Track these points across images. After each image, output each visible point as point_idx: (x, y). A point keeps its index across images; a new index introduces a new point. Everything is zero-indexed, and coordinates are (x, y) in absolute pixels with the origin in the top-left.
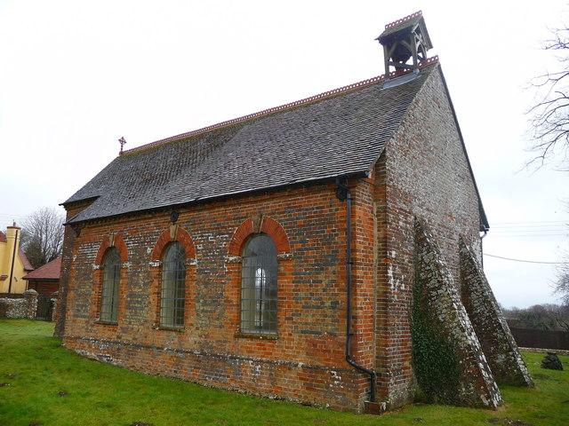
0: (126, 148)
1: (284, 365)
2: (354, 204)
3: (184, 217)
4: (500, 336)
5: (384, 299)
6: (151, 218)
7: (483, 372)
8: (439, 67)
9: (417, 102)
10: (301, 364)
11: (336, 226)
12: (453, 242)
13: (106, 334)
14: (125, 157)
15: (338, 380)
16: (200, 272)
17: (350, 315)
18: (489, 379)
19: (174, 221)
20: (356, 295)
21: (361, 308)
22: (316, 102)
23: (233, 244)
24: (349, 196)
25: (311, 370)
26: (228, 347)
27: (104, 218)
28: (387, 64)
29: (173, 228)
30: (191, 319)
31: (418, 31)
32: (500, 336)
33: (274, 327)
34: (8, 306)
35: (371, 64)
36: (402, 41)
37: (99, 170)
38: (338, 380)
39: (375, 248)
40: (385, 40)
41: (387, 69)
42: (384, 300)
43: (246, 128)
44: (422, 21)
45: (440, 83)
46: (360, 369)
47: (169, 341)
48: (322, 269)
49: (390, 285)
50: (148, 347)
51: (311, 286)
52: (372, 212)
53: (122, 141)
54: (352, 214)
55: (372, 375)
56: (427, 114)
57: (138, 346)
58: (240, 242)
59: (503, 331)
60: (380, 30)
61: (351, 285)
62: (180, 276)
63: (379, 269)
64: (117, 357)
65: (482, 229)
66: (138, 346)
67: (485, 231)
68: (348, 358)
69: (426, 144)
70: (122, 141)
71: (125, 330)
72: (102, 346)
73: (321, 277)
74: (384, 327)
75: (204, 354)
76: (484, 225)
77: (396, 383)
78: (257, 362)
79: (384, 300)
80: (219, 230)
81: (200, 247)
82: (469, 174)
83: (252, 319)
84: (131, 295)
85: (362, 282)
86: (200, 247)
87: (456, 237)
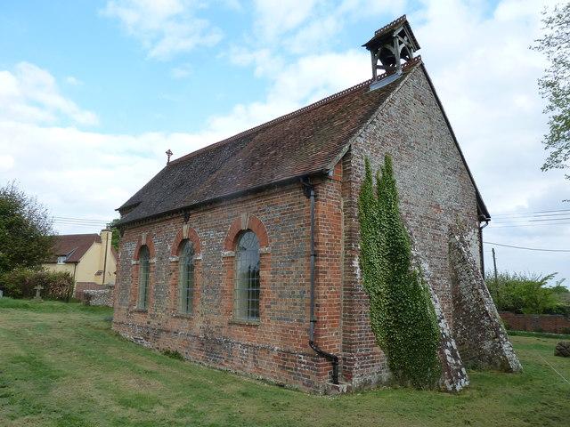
0: (173, 159)
1: (264, 348)
2: (317, 200)
3: (194, 217)
4: (487, 323)
5: (350, 289)
6: (170, 219)
7: (449, 359)
8: (422, 65)
9: (392, 101)
10: (276, 348)
11: (304, 222)
12: (439, 232)
13: (140, 319)
14: (172, 166)
15: (304, 363)
16: (204, 266)
17: (314, 306)
18: (457, 365)
19: (187, 220)
20: (319, 285)
21: (325, 297)
22: (343, 97)
23: (227, 240)
24: (312, 193)
25: (285, 355)
26: (224, 331)
27: (143, 219)
28: (375, 67)
29: (185, 227)
30: (199, 307)
31: (402, 34)
32: (487, 323)
33: (256, 314)
34: (91, 296)
35: (358, 69)
36: (391, 45)
37: (156, 174)
38: (304, 363)
39: (342, 241)
40: (371, 46)
41: (374, 72)
42: (349, 290)
43: (258, 137)
44: (406, 24)
45: (424, 81)
46: (322, 354)
47: (183, 327)
48: (293, 261)
49: (356, 275)
50: (168, 332)
51: (284, 277)
52: (339, 207)
53: (169, 153)
54: (315, 210)
55: (336, 359)
56: (406, 111)
57: (161, 331)
58: (232, 238)
59: (490, 319)
60: (370, 36)
61: (315, 274)
62: (190, 268)
63: (345, 260)
64: (146, 339)
65: (481, 220)
66: (161, 331)
67: (487, 221)
68: (311, 343)
69: (404, 141)
70: (169, 153)
71: (153, 317)
72: (138, 331)
73: (292, 268)
74: (349, 315)
75: (206, 338)
76: (483, 214)
77: (362, 367)
78: (245, 346)
79: (349, 290)
80: (218, 228)
81: (204, 243)
82: (463, 166)
83: (239, 304)
84: (157, 286)
85: (326, 273)
86: (204, 243)
87: (445, 228)
